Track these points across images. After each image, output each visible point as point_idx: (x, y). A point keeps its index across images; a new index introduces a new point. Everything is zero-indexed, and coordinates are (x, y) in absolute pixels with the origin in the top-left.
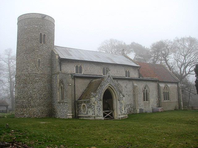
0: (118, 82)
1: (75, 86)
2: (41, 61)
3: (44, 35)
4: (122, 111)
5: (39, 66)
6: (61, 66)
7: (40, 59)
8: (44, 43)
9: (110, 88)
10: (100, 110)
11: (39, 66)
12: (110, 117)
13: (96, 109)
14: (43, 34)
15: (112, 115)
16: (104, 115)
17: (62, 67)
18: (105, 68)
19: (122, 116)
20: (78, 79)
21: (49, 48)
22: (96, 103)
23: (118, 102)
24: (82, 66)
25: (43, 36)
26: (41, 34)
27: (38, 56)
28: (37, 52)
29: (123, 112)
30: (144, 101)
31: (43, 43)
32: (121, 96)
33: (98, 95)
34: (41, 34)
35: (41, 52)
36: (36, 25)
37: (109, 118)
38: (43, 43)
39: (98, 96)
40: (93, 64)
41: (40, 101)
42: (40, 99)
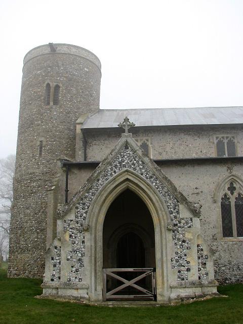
0: (234, 173)
1: (67, 191)
2: (44, 143)
3: (57, 87)
4: (188, 270)
5: (40, 154)
6: (85, 150)
7: (43, 139)
8: (56, 102)
9: (133, 187)
10: (82, 266)
11: (40, 154)
12: (140, 292)
13: (63, 261)
14: (53, 85)
15: (147, 283)
16: (111, 284)
17: (88, 150)
18: (226, 141)
19: (184, 293)
20: (82, 171)
21: (69, 113)
22: (67, 237)
23: (170, 236)
24: (149, 143)
25: (52, 90)
26: (48, 85)
27: (39, 135)
28: (39, 125)
29: (193, 276)
30: (231, 235)
31: (52, 103)
32: (185, 213)
33: (74, 211)
34: (48, 85)
35: (47, 124)
36: (38, 70)
37: (132, 296)
38: (52, 103)
39: (76, 217)
40: (182, 135)
41: (37, 238)
42: (38, 233)
